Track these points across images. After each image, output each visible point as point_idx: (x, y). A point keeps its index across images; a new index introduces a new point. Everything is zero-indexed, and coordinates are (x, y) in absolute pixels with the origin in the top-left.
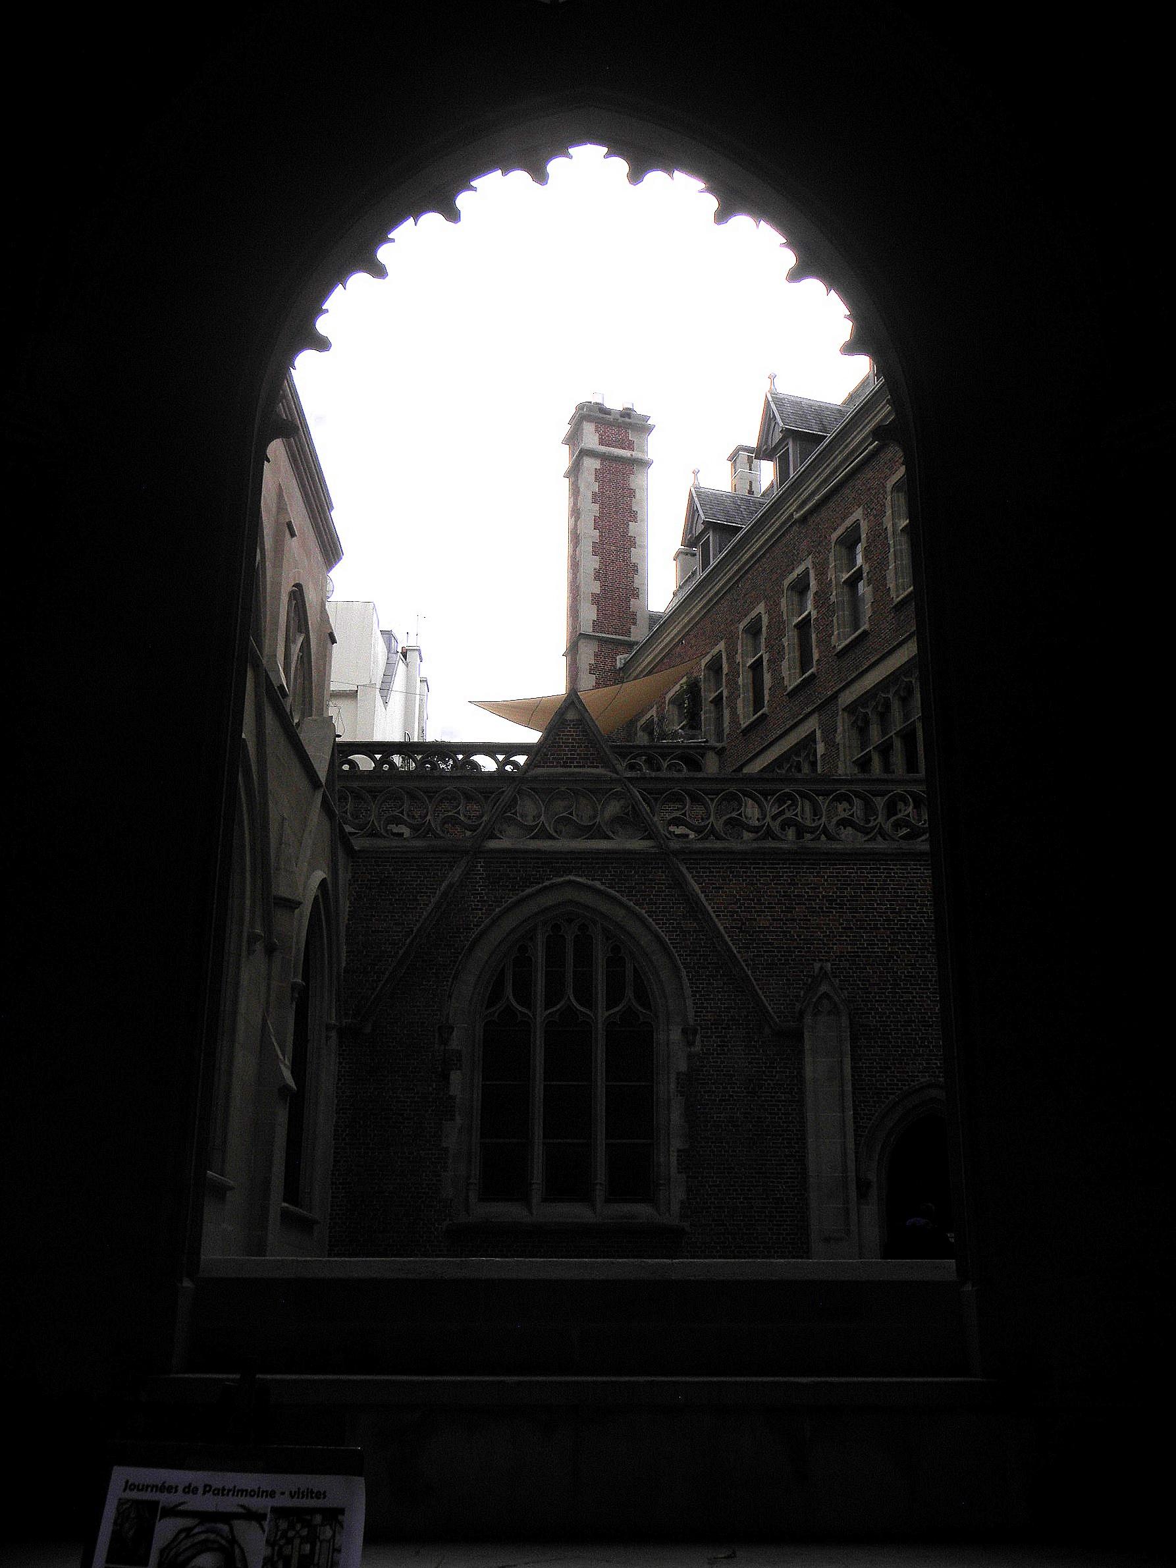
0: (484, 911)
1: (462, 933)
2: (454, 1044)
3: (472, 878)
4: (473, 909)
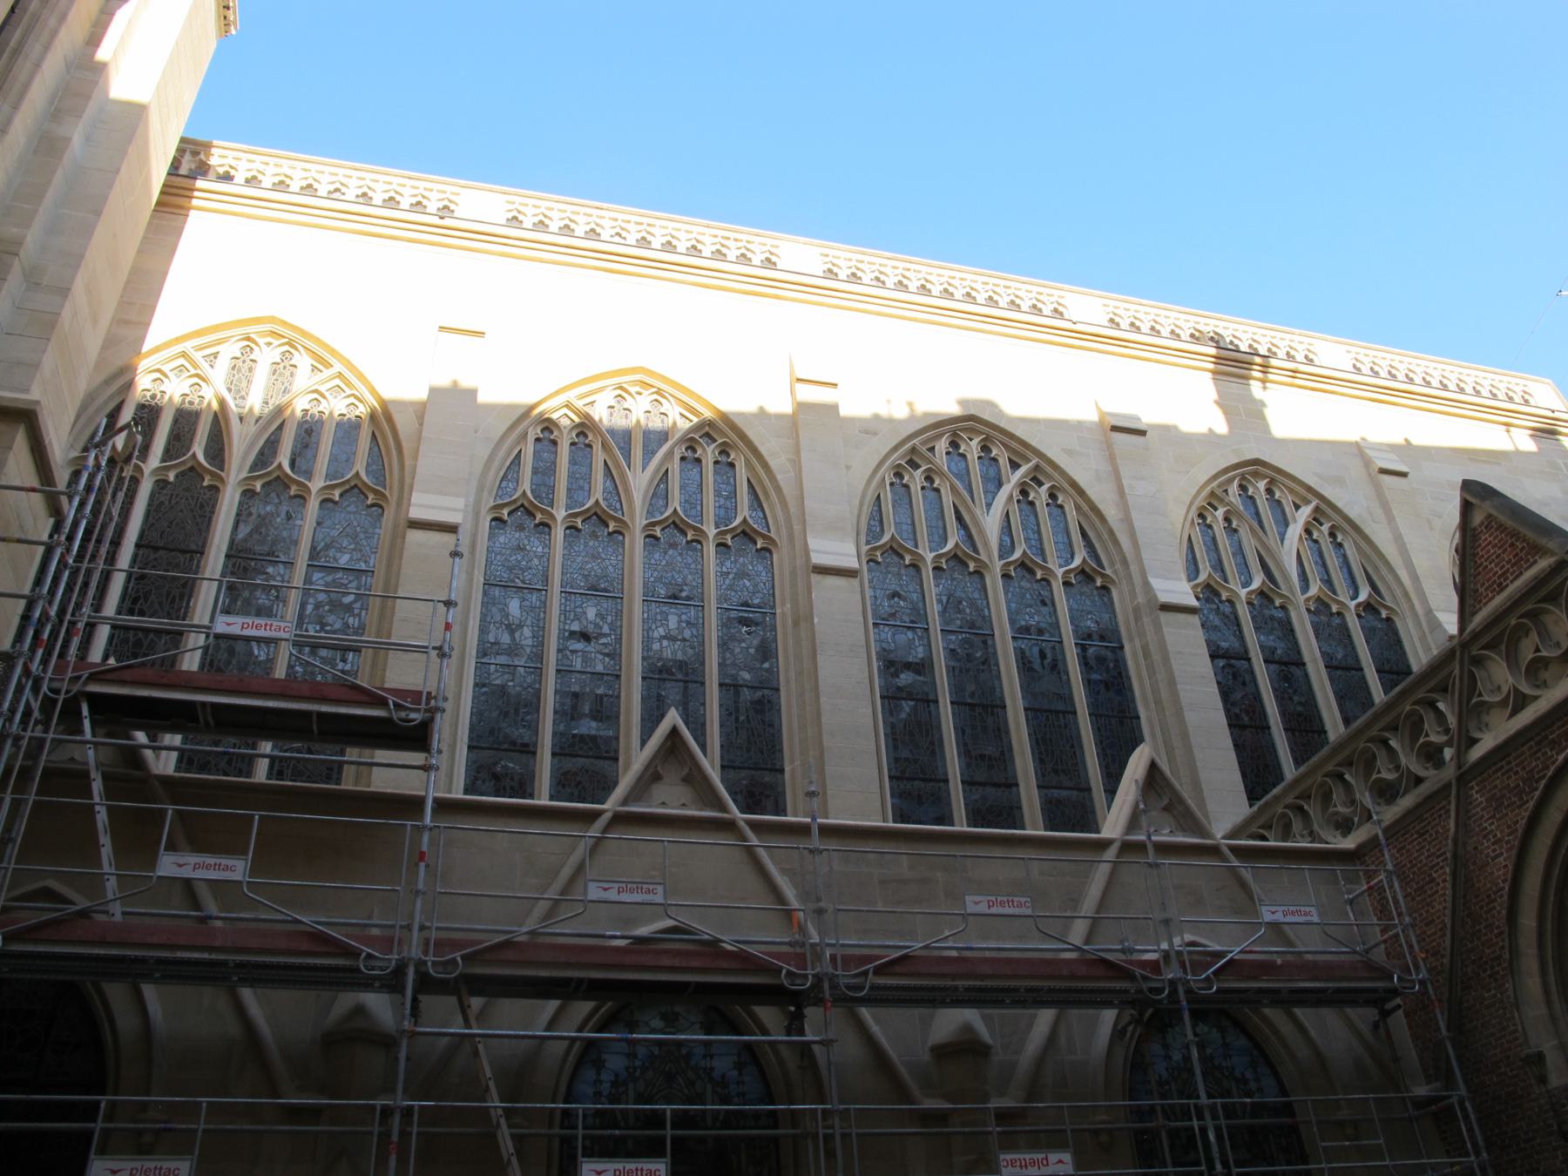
1: (1495, 900)
3: (1474, 815)
4: (1494, 859)
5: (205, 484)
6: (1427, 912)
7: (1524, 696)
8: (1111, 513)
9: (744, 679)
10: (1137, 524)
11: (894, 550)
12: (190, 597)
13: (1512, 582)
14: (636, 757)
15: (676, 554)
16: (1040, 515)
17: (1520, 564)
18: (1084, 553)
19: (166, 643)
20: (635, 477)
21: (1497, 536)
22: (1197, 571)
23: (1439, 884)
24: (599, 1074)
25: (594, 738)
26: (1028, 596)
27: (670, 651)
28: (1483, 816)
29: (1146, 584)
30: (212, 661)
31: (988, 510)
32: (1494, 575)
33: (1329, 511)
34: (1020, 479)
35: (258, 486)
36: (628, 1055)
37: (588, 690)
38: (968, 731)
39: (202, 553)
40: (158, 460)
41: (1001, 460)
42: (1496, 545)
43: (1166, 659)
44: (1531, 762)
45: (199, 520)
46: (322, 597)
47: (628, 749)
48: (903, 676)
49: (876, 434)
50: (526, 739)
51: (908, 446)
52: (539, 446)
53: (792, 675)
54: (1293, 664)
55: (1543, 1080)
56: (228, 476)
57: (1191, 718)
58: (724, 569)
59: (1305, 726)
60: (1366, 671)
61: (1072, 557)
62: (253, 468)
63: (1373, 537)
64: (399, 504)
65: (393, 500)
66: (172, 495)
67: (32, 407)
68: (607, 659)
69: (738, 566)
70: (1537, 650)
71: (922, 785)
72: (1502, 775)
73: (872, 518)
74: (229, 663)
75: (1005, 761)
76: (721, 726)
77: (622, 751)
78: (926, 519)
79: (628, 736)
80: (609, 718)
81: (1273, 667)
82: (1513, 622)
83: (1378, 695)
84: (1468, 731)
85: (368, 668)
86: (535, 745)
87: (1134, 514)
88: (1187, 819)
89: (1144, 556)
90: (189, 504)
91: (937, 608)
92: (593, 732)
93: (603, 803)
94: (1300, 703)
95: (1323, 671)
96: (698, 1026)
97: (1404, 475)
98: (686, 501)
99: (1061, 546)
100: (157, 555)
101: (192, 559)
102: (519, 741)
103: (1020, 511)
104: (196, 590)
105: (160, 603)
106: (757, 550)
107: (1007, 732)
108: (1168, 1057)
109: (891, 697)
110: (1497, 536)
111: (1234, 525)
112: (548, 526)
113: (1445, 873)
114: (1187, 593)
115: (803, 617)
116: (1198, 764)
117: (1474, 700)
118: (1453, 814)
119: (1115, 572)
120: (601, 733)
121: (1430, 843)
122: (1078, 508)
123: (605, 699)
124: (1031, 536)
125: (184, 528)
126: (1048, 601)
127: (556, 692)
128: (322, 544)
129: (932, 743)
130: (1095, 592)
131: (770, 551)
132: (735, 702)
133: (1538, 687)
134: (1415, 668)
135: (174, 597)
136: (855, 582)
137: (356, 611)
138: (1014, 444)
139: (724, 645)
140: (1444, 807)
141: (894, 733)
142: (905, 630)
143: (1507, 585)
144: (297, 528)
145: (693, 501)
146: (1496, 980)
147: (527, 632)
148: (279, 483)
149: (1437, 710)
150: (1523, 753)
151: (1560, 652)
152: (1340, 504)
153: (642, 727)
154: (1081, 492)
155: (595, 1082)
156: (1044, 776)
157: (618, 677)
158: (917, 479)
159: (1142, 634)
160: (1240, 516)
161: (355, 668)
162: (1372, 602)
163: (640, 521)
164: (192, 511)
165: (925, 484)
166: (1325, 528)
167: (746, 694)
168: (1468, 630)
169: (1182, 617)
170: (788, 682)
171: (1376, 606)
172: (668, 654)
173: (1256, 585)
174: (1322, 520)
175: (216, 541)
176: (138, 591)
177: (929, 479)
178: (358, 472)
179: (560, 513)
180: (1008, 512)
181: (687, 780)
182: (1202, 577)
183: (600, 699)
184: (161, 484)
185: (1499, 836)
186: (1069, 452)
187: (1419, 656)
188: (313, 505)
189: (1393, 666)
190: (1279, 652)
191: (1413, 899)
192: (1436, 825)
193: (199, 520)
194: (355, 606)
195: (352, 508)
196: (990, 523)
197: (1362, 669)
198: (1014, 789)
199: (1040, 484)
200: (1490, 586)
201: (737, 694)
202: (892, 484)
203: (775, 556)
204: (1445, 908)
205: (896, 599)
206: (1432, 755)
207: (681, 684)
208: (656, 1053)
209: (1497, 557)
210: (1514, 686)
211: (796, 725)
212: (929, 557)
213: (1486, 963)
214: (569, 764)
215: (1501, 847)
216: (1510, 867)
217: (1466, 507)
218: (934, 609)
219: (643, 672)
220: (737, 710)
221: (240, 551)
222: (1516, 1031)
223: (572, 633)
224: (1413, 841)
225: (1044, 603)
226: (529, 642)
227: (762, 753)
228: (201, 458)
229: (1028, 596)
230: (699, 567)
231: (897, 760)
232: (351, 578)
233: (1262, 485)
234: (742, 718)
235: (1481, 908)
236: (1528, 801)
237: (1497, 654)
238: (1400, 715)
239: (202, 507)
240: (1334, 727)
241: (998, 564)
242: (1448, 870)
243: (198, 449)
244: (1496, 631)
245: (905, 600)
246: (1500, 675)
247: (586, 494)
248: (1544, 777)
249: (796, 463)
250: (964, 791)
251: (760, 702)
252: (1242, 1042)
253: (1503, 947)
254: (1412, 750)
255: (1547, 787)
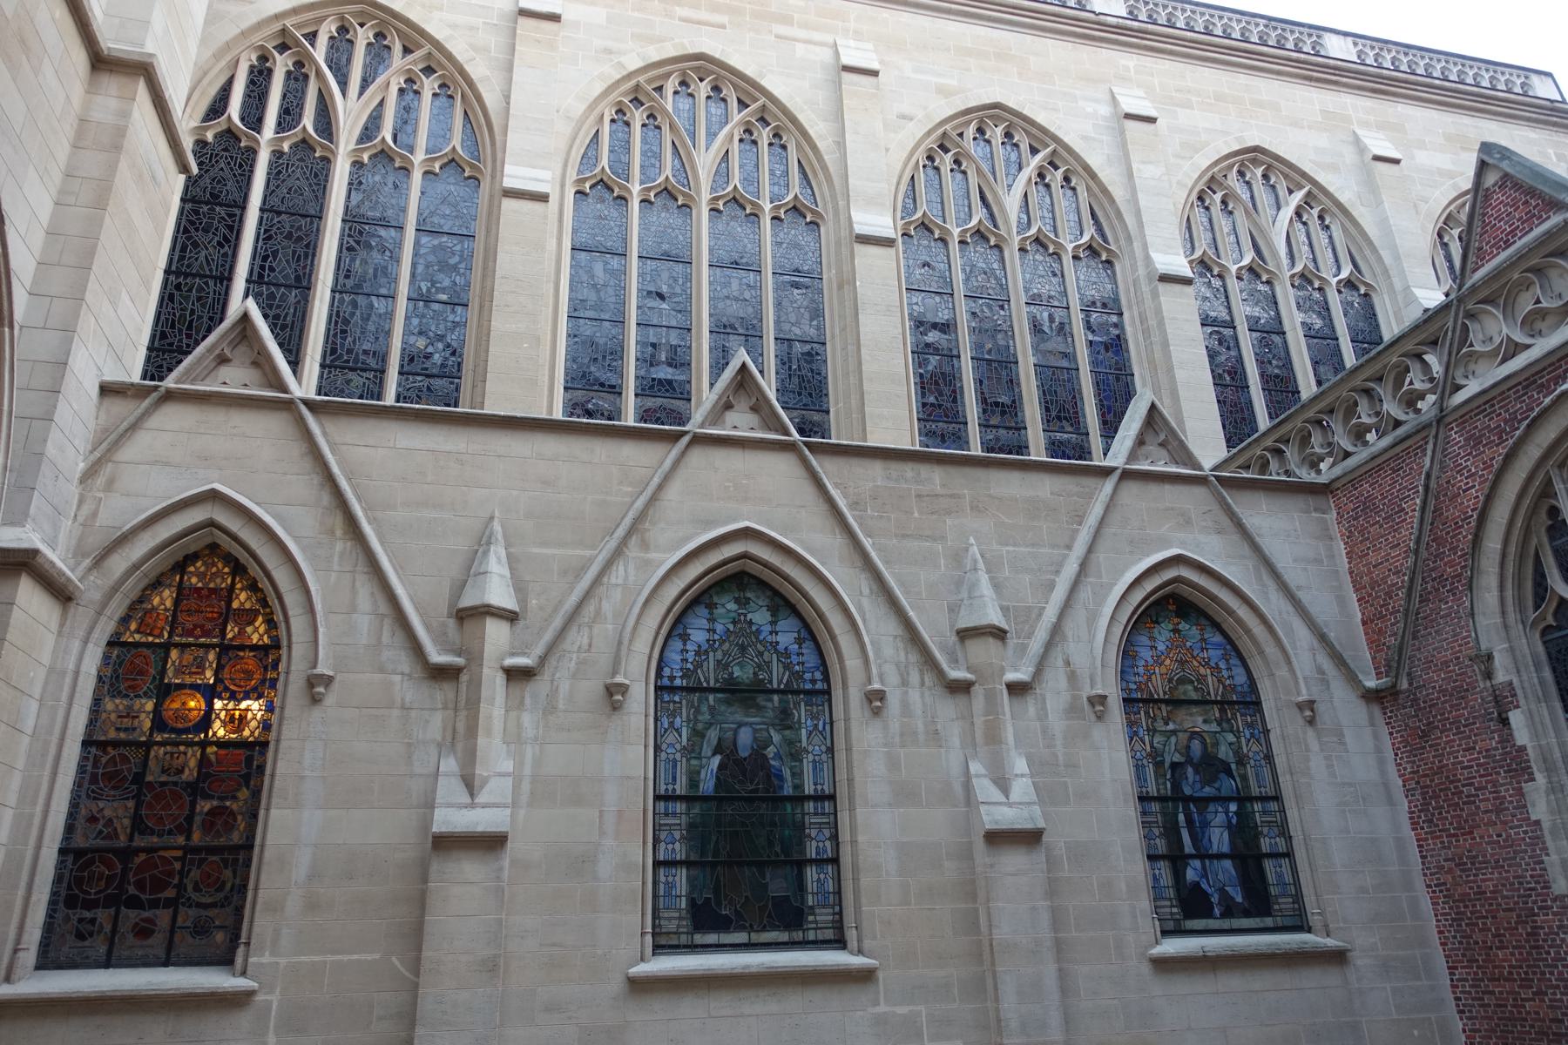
0: (1477, 487)
1: (1462, 526)
2: (1501, 677)
3: (1450, 453)
4: (1464, 491)
5: (317, 155)
6: (1393, 537)
7: (1517, 344)
8: (1118, 192)
9: (795, 335)
10: (1142, 203)
11: (924, 226)
12: (314, 255)
13: (1520, 238)
14: (706, 394)
15: (736, 224)
16: (1054, 195)
17: (1530, 220)
18: (1093, 230)
19: (296, 296)
20: (699, 156)
21: (1511, 195)
22: (1193, 248)
23: (1407, 513)
24: (685, 645)
25: (670, 382)
26: (1041, 268)
27: (734, 310)
28: (1459, 454)
29: (1148, 258)
30: (338, 312)
31: (1009, 190)
32: (1502, 233)
33: (1321, 196)
34: (1040, 161)
35: (366, 158)
36: (709, 630)
37: (664, 341)
38: (985, 382)
39: (320, 218)
40: (272, 132)
41: (1022, 146)
42: (1508, 204)
43: (1161, 324)
44: (1516, 405)
45: (315, 188)
46: (431, 258)
47: (699, 390)
48: (930, 334)
49: (911, 119)
50: (613, 382)
51: (940, 131)
52: (614, 126)
53: (837, 331)
54: (1274, 333)
55: (1489, 675)
56: (337, 147)
57: (1180, 375)
58: (779, 240)
59: (1281, 386)
60: (1341, 340)
61: (1081, 234)
62: (361, 140)
63: (1360, 220)
64: (493, 177)
65: (488, 171)
66: (288, 164)
67: (149, 60)
68: (679, 316)
69: (790, 236)
70: (1538, 301)
71: (945, 426)
72: (1484, 417)
73: (906, 196)
74: (353, 314)
75: (1015, 408)
76: (777, 373)
77: (693, 392)
78: (954, 198)
79: (699, 379)
80: (682, 365)
81: (1255, 335)
82: (1516, 276)
83: (1350, 360)
84: (1454, 378)
85: (475, 319)
86: (621, 387)
87: (1140, 195)
88: (1182, 453)
89: (1146, 232)
90: (304, 173)
91: (961, 276)
92: (669, 377)
93: (684, 426)
94: (1277, 367)
95: (1303, 340)
96: (765, 609)
97: (1397, 162)
98: (745, 179)
99: (1072, 224)
100: (279, 219)
101: (312, 223)
102: (607, 383)
103: (1038, 192)
104: (318, 250)
105: (287, 261)
106: (806, 224)
107: (1019, 385)
108: (1153, 647)
109: (922, 352)
110: (1511, 195)
111: (1230, 208)
112: (625, 199)
113: (1415, 504)
114: (1185, 267)
115: (847, 282)
116: (1185, 415)
117: (1464, 350)
118: (1429, 453)
119: (1119, 247)
120: (676, 378)
121: (1402, 479)
122: (1089, 189)
123: (679, 349)
124: (1046, 215)
125: (302, 194)
126: (1059, 273)
127: (637, 343)
128: (428, 211)
129: (954, 391)
130: (1100, 266)
131: (818, 225)
132: (788, 354)
133: (1533, 336)
134: (1387, 336)
135: (299, 256)
136: (892, 251)
137: (462, 271)
138: (1034, 131)
139: (778, 305)
140: (1421, 446)
141: (922, 383)
142: (933, 295)
143: (1515, 241)
144: (404, 196)
145: (752, 180)
146: (1454, 595)
147: (611, 291)
148: (384, 155)
149: (1424, 362)
150: (1508, 397)
151: (1561, 303)
152: (1331, 189)
153: (711, 372)
154: (1093, 175)
155: (682, 651)
156: (1048, 421)
157: (689, 330)
158: (947, 162)
159: (1140, 302)
160: (1237, 199)
161: (464, 320)
162: (1353, 279)
163: (706, 196)
164: (307, 178)
165: (954, 167)
166: (1315, 212)
167: (798, 348)
168: (1466, 287)
169: (1178, 288)
170: (833, 337)
171: (1357, 283)
172: (729, 311)
173: (1246, 261)
174: (1313, 204)
175: (332, 206)
176: (266, 250)
177: (957, 162)
178: (454, 147)
179: (636, 188)
180: (1026, 193)
181: (754, 409)
182: (1198, 253)
183: (674, 349)
184: (277, 154)
185: (1473, 470)
186: (1085, 138)
187: (1390, 328)
188: (417, 176)
189: (1367, 334)
190: (1262, 321)
191: (1381, 526)
192: (1411, 462)
193: (315, 188)
194: (460, 266)
195: (452, 180)
196: (1011, 203)
197: (1337, 339)
198: (1023, 432)
199: (1056, 168)
200: (1496, 244)
201: (790, 347)
202: (924, 166)
203: (822, 229)
204: (1411, 534)
205: (926, 268)
206: (1411, 401)
207: (743, 338)
208: (732, 629)
209: (1507, 215)
210: (1508, 336)
211: (839, 372)
212: (956, 232)
213: (1447, 579)
214: (651, 403)
215: (1475, 481)
216: (1481, 498)
217: (1482, 166)
218: (959, 277)
219: (710, 327)
220: (790, 360)
221: (354, 217)
222: (1470, 636)
223: (649, 293)
224: (1387, 476)
225: (1055, 275)
226: (613, 299)
227: (811, 397)
228: (311, 130)
229: (1041, 268)
230: (757, 237)
231: (924, 405)
232: (455, 242)
233: (1259, 172)
234: (794, 367)
235: (1448, 533)
236: (1507, 440)
237: (1493, 307)
238: (1385, 366)
239: (316, 175)
240: (1307, 386)
241: (1017, 239)
242: (1418, 501)
243: (308, 122)
244: (1495, 286)
245: (934, 269)
246: (1495, 327)
247: (658, 171)
248: (1527, 418)
249: (841, 145)
250: (980, 432)
251: (809, 354)
252: (1218, 638)
253: (1465, 566)
254: (1394, 397)
255: (1528, 426)
